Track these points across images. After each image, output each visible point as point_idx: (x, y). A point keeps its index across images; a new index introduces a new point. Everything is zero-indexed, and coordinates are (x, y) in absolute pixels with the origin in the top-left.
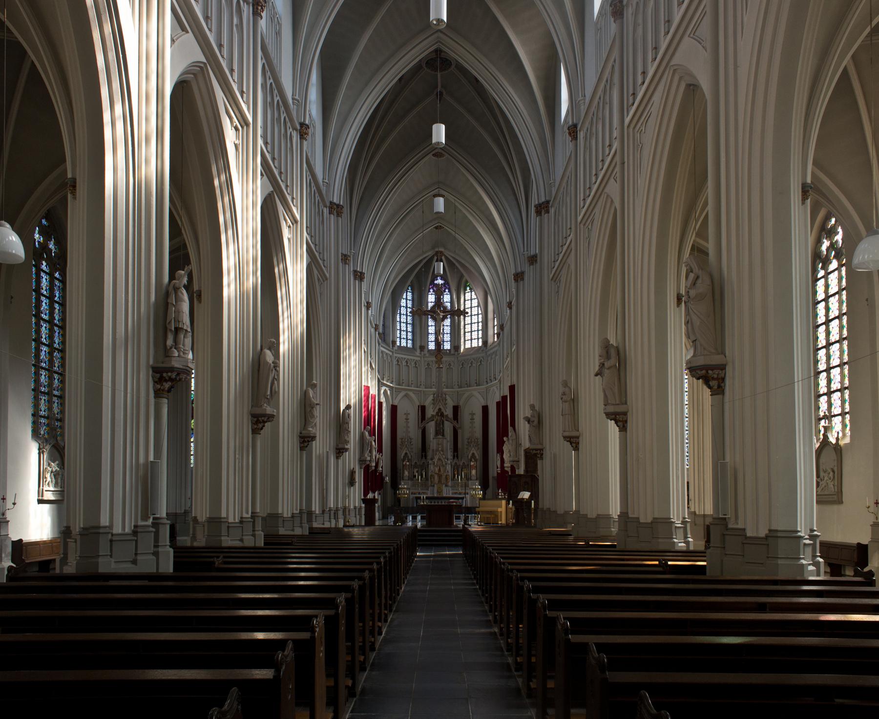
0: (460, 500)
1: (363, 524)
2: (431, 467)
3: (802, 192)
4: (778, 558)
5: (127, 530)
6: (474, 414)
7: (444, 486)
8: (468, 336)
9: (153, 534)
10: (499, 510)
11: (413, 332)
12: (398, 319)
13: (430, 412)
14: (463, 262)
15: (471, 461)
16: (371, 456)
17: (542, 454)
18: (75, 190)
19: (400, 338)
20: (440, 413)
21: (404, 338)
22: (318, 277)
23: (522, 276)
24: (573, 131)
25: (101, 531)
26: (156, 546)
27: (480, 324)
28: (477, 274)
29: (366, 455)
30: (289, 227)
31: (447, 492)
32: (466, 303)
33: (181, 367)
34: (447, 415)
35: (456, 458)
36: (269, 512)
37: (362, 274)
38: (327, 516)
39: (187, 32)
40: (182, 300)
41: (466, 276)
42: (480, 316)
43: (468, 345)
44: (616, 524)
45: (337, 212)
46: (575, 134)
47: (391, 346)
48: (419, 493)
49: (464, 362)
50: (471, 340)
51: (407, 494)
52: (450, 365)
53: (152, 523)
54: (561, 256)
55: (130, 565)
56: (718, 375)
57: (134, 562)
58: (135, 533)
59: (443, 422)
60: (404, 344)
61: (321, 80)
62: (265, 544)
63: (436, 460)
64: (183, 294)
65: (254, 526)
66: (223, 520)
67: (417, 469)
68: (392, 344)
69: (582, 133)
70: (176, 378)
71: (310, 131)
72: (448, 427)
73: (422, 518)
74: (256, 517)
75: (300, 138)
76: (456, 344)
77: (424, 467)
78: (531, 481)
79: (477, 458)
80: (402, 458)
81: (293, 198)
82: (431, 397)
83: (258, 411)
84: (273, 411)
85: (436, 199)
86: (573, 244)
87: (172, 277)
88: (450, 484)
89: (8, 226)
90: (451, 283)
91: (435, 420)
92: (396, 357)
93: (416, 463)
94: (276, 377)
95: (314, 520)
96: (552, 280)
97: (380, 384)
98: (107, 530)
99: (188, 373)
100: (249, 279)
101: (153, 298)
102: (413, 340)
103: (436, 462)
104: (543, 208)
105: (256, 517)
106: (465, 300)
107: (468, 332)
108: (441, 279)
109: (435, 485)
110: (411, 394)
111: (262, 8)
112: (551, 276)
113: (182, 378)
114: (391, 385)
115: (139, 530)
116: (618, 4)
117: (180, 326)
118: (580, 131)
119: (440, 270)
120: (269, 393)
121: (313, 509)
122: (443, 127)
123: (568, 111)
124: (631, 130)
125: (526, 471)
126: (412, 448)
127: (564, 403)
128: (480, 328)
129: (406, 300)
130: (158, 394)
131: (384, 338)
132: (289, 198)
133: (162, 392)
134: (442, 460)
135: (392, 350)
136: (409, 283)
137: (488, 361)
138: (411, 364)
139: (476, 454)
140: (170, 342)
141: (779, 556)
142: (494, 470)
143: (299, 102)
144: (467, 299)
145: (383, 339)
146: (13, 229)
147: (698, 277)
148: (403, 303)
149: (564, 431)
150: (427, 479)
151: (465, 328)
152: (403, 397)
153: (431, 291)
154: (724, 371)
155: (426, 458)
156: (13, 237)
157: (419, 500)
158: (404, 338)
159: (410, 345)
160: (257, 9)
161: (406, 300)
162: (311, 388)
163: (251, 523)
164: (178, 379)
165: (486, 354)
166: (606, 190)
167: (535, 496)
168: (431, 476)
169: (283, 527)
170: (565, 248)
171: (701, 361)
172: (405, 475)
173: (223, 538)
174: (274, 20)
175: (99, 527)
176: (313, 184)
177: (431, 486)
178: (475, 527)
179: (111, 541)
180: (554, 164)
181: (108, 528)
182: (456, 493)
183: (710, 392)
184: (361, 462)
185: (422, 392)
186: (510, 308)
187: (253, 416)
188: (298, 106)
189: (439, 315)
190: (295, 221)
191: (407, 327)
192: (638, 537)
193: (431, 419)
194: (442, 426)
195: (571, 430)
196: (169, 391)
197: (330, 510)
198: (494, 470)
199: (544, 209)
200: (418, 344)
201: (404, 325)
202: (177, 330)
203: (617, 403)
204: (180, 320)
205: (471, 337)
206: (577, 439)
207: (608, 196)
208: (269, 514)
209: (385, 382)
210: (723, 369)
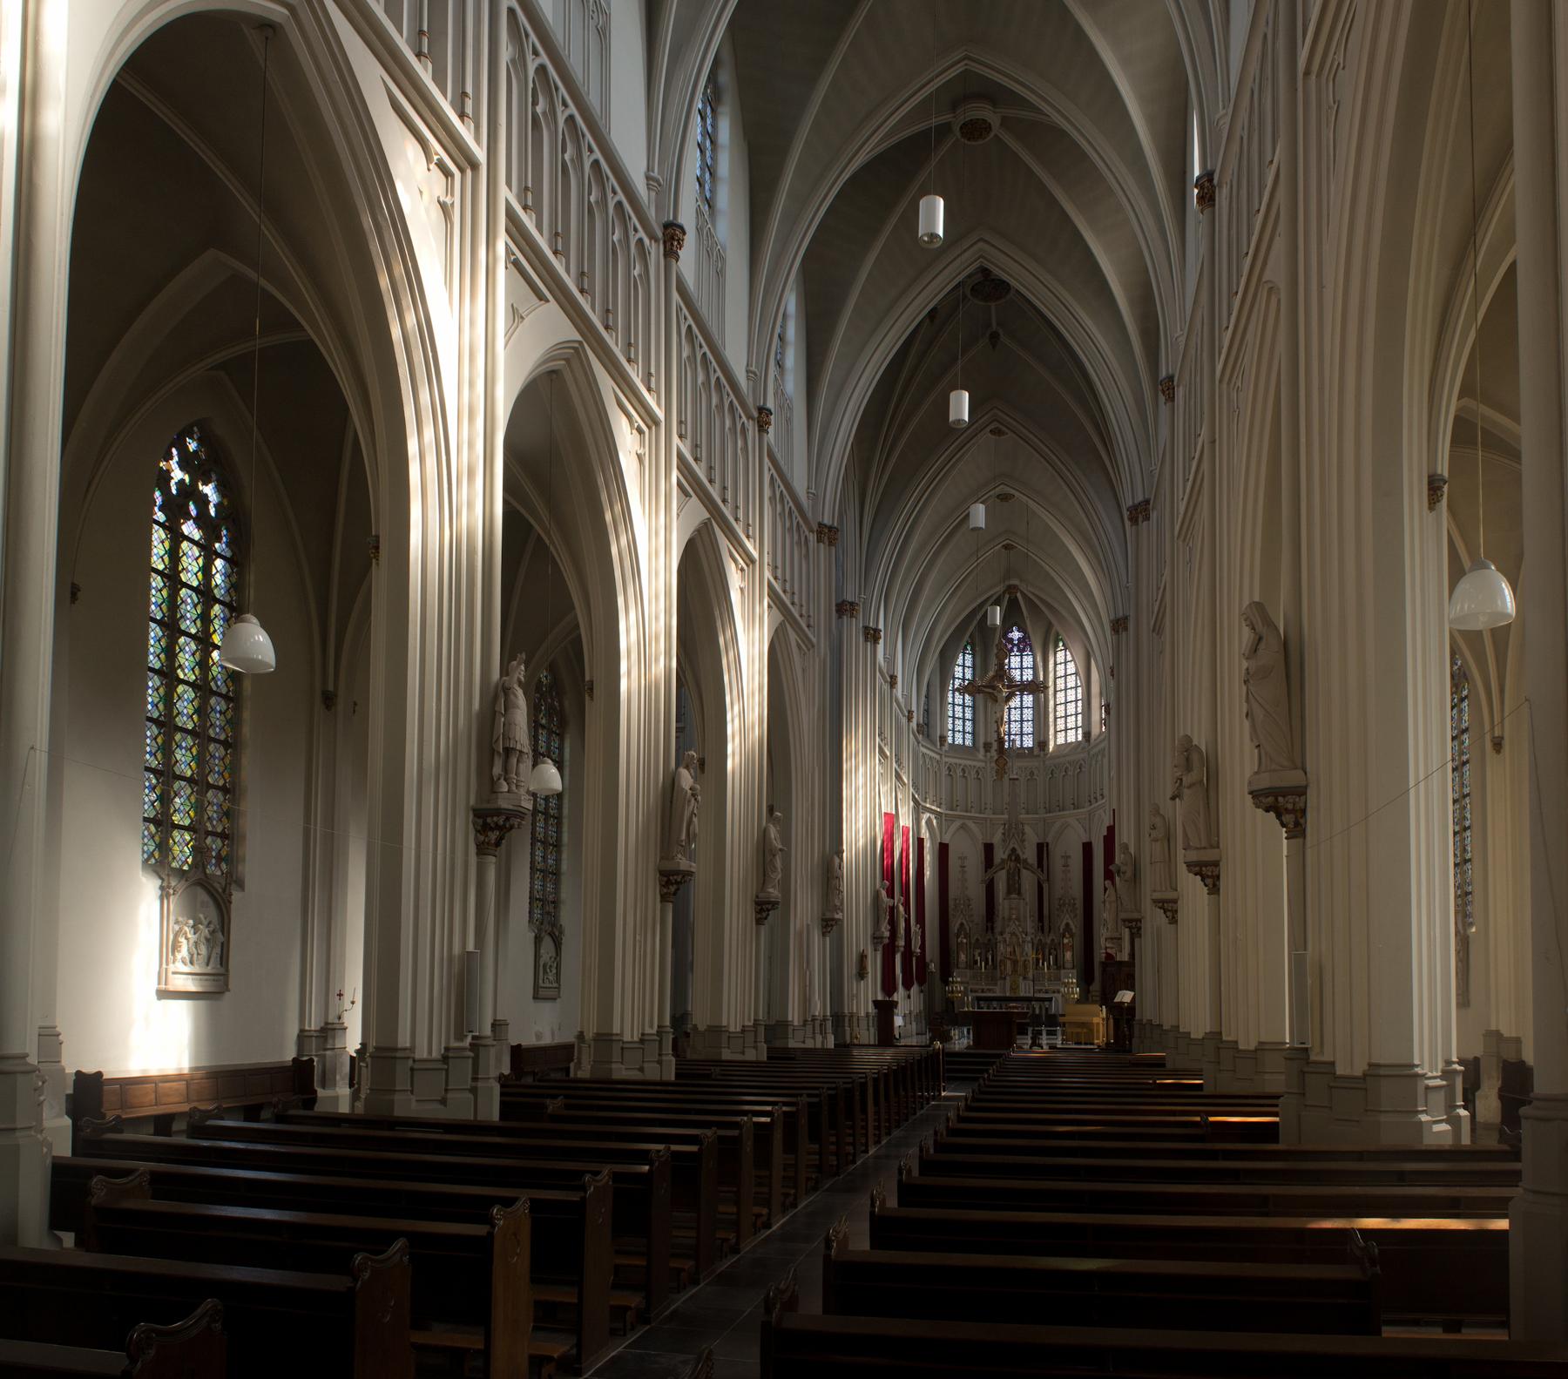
0: (1046, 1003)
2: (1001, 947)
3: (1429, 490)
4: (1381, 1112)
5: (435, 1055)
6: (1069, 857)
7: (1021, 978)
8: (1061, 724)
9: (470, 1061)
10: (1096, 1020)
11: (974, 720)
13: (1000, 855)
14: (1049, 600)
15: (1064, 936)
17: (1140, 928)
18: (378, 552)
19: (953, 731)
20: (1014, 856)
21: (959, 731)
22: (797, 642)
23: (1124, 623)
25: (399, 1054)
26: (475, 1079)
27: (1080, 703)
29: (883, 929)
31: (1025, 990)
32: (1057, 669)
33: (511, 807)
34: (1026, 859)
35: (990, 932)
36: (708, 1024)
37: (877, 631)
38: (809, 1028)
39: (547, 301)
40: (516, 706)
41: (1057, 627)
42: (1079, 690)
43: (1061, 741)
45: (829, 538)
46: (1171, 391)
47: (938, 744)
49: (1083, 762)
50: (1066, 731)
51: (960, 992)
52: (1032, 773)
53: (470, 1044)
55: (438, 1106)
56: (1294, 805)
57: (443, 1102)
58: (445, 1059)
59: (1019, 870)
60: (959, 741)
61: (805, 333)
62: (677, 1075)
63: (1007, 936)
64: (516, 696)
65: (660, 1048)
66: (614, 1038)
67: (979, 951)
68: (940, 741)
69: (1181, 388)
70: (504, 825)
72: (1028, 881)
74: (481, 1048)
75: (759, 431)
76: (1042, 739)
77: (990, 947)
79: (1074, 931)
80: (956, 931)
82: (1001, 830)
83: (669, 866)
84: (691, 866)
87: (505, 671)
88: (1030, 975)
89: (255, 620)
90: (1032, 638)
91: (1007, 867)
92: (946, 763)
93: (977, 940)
94: (695, 812)
95: (790, 1036)
96: (1153, 631)
97: (918, 809)
98: (407, 1054)
99: (523, 815)
100: (659, 661)
101: (476, 705)
102: (974, 733)
103: (1008, 939)
104: (1140, 512)
105: (664, 1034)
106: (1056, 664)
107: (1061, 717)
108: (1019, 631)
109: (1008, 978)
110: (970, 824)
111: (679, 243)
113: (514, 824)
114: (938, 810)
115: (451, 1055)
116: (1206, 184)
117: (511, 746)
118: (1178, 386)
119: (996, 621)
120: (683, 837)
121: (790, 1019)
122: (967, 394)
124: (1225, 386)
126: (972, 915)
127: (1153, 843)
128: (1079, 710)
129: (964, 667)
130: (482, 850)
131: (928, 731)
133: (486, 846)
134: (1017, 936)
135: (939, 751)
136: (966, 637)
137: (1091, 765)
138: (969, 773)
139: (1073, 927)
140: (497, 770)
141: (1382, 1109)
143: (756, 375)
144: (1058, 661)
145: (925, 733)
146: (263, 626)
147: (1260, 639)
149: (1155, 891)
150: (994, 967)
151: (1055, 711)
152: (958, 829)
154: (1303, 798)
155: (993, 932)
156: (260, 637)
158: (959, 731)
159: (968, 742)
160: (672, 245)
162: (774, 824)
163: (657, 1043)
164: (507, 826)
165: (1089, 754)
168: (1001, 961)
169: (729, 1048)
171: (1265, 782)
172: (960, 960)
173: (614, 1066)
174: (713, 255)
175: (396, 1049)
177: (1001, 978)
179: (412, 1069)
180: (1157, 440)
181: (408, 1051)
182: (1040, 991)
183: (1286, 832)
184: (876, 941)
185: (988, 821)
187: (663, 873)
189: (1001, 691)
191: (964, 712)
192: (1234, 1071)
193: (1001, 867)
194: (1017, 878)
195: (1164, 889)
196: (498, 844)
197: (813, 1020)
199: (1141, 513)
200: (981, 741)
201: (959, 723)
202: (508, 751)
203: (1203, 845)
204: (510, 737)
205: (1066, 725)
206: (1173, 905)
208: (708, 1026)
209: (928, 806)
210: (1302, 795)
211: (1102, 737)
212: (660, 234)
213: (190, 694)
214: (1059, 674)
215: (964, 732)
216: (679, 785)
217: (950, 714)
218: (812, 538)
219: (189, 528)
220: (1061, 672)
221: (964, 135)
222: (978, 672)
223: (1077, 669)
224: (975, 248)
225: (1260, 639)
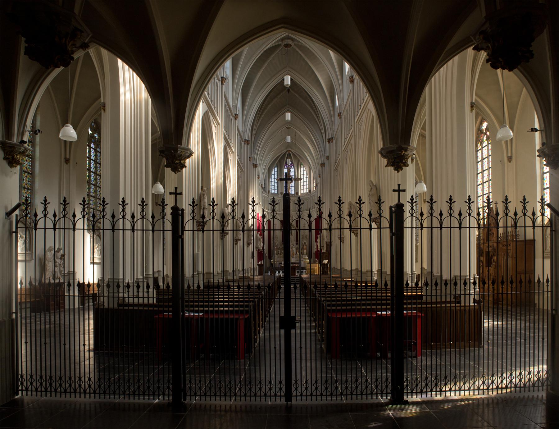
1: (258, 275)
10: (316, 268)
11: (277, 186)
12: (271, 180)
14: (299, 154)
15: (304, 246)
16: (260, 245)
19: (272, 189)
24: (340, 115)
27: (308, 182)
28: (306, 160)
30: (216, 127)
40: (205, 198)
42: (308, 178)
43: (302, 192)
44: (376, 275)
48: (281, 261)
54: (348, 139)
60: (273, 192)
71: (227, 80)
73: (282, 272)
74: (149, 278)
78: (328, 256)
81: (218, 113)
85: (286, 114)
86: (341, 159)
88: (294, 256)
102: (277, 190)
104: (330, 140)
106: (301, 171)
112: (334, 168)
123: (349, 70)
124: (357, 124)
125: (327, 251)
128: (308, 184)
129: (275, 171)
132: (216, 113)
139: (306, 243)
142: (314, 250)
147: (372, 188)
148: (273, 173)
151: (301, 184)
153: (286, 167)
157: (281, 264)
159: (276, 192)
161: (275, 171)
166: (368, 107)
167: (330, 261)
170: (349, 135)
176: (227, 106)
178: (305, 275)
186: (341, 118)
188: (234, 108)
190: (218, 124)
198: (314, 250)
201: (273, 187)
207: (369, 109)
211: (314, 192)
212: (221, 79)
213: (93, 187)
214: (301, 174)
215: (275, 189)
216: (225, 212)
217: (271, 184)
218: (243, 143)
219: (92, 145)
220: (302, 173)
221: (284, 47)
222: (279, 173)
223: (307, 172)
224: (286, 72)
225: (372, 188)
